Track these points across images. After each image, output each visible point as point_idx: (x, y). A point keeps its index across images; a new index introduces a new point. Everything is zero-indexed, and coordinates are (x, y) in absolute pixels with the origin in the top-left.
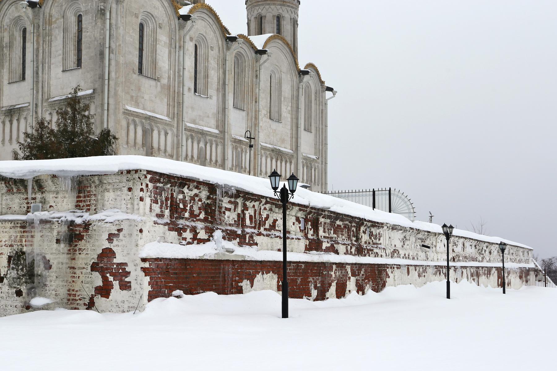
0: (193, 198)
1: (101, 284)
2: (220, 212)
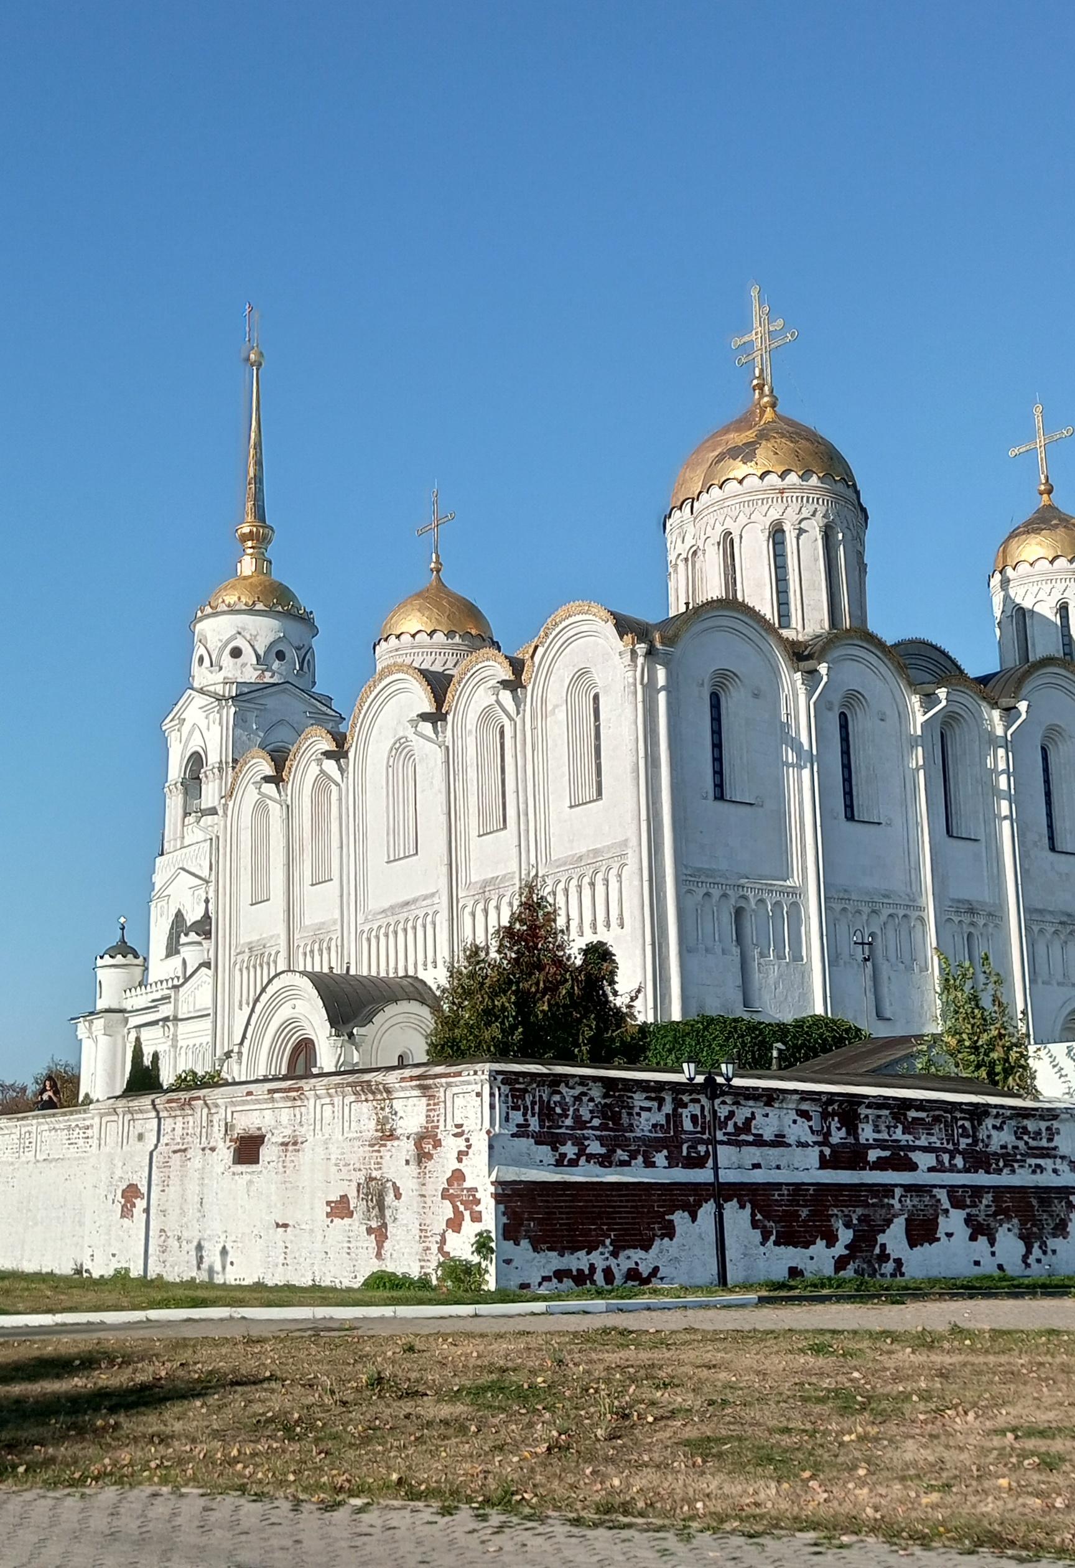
0: (578, 1098)
1: (452, 1216)
2: (630, 1114)
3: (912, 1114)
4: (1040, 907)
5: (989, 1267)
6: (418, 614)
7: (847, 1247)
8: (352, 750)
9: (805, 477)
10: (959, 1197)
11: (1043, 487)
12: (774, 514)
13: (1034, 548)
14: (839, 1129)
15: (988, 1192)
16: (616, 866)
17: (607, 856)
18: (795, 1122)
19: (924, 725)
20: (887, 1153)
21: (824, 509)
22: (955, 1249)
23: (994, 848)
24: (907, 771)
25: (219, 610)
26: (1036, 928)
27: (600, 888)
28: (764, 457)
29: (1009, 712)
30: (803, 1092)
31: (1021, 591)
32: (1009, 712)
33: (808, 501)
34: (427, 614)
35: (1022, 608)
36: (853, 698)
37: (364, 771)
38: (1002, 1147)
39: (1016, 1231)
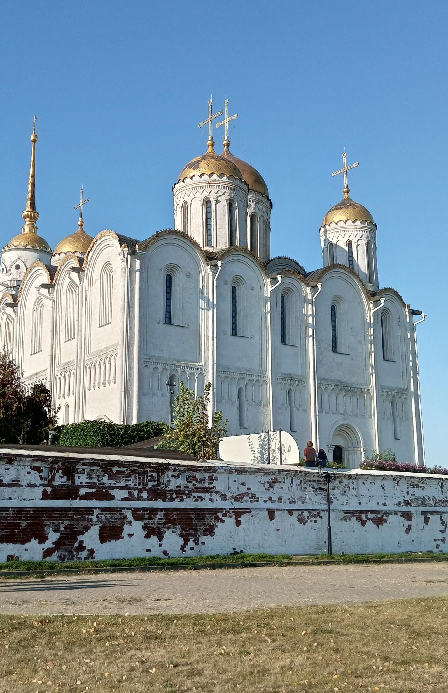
3: (115, 469)
4: (327, 377)
5: (157, 552)
6: (69, 244)
7: (53, 543)
8: (20, 303)
9: (220, 177)
10: (138, 514)
11: (345, 190)
12: (206, 193)
13: (339, 216)
14: (61, 477)
15: (162, 511)
16: (114, 354)
17: (111, 350)
18: (29, 473)
19: (273, 292)
20: (94, 490)
21: (229, 191)
22: (134, 542)
23: (304, 350)
24: (263, 314)
25: (11, 248)
26: (323, 388)
27: (108, 365)
28: (203, 167)
29: (314, 287)
30: (34, 456)
31: (332, 236)
32: (314, 287)
33: (221, 188)
34: (73, 244)
35: (332, 244)
36: (238, 280)
37: (24, 312)
38: (177, 487)
39: (179, 532)
